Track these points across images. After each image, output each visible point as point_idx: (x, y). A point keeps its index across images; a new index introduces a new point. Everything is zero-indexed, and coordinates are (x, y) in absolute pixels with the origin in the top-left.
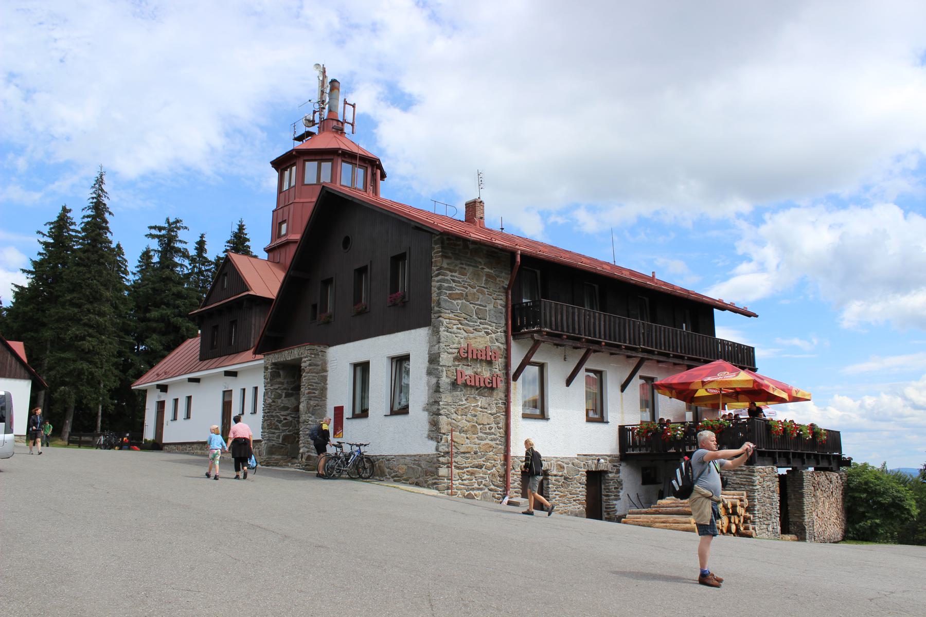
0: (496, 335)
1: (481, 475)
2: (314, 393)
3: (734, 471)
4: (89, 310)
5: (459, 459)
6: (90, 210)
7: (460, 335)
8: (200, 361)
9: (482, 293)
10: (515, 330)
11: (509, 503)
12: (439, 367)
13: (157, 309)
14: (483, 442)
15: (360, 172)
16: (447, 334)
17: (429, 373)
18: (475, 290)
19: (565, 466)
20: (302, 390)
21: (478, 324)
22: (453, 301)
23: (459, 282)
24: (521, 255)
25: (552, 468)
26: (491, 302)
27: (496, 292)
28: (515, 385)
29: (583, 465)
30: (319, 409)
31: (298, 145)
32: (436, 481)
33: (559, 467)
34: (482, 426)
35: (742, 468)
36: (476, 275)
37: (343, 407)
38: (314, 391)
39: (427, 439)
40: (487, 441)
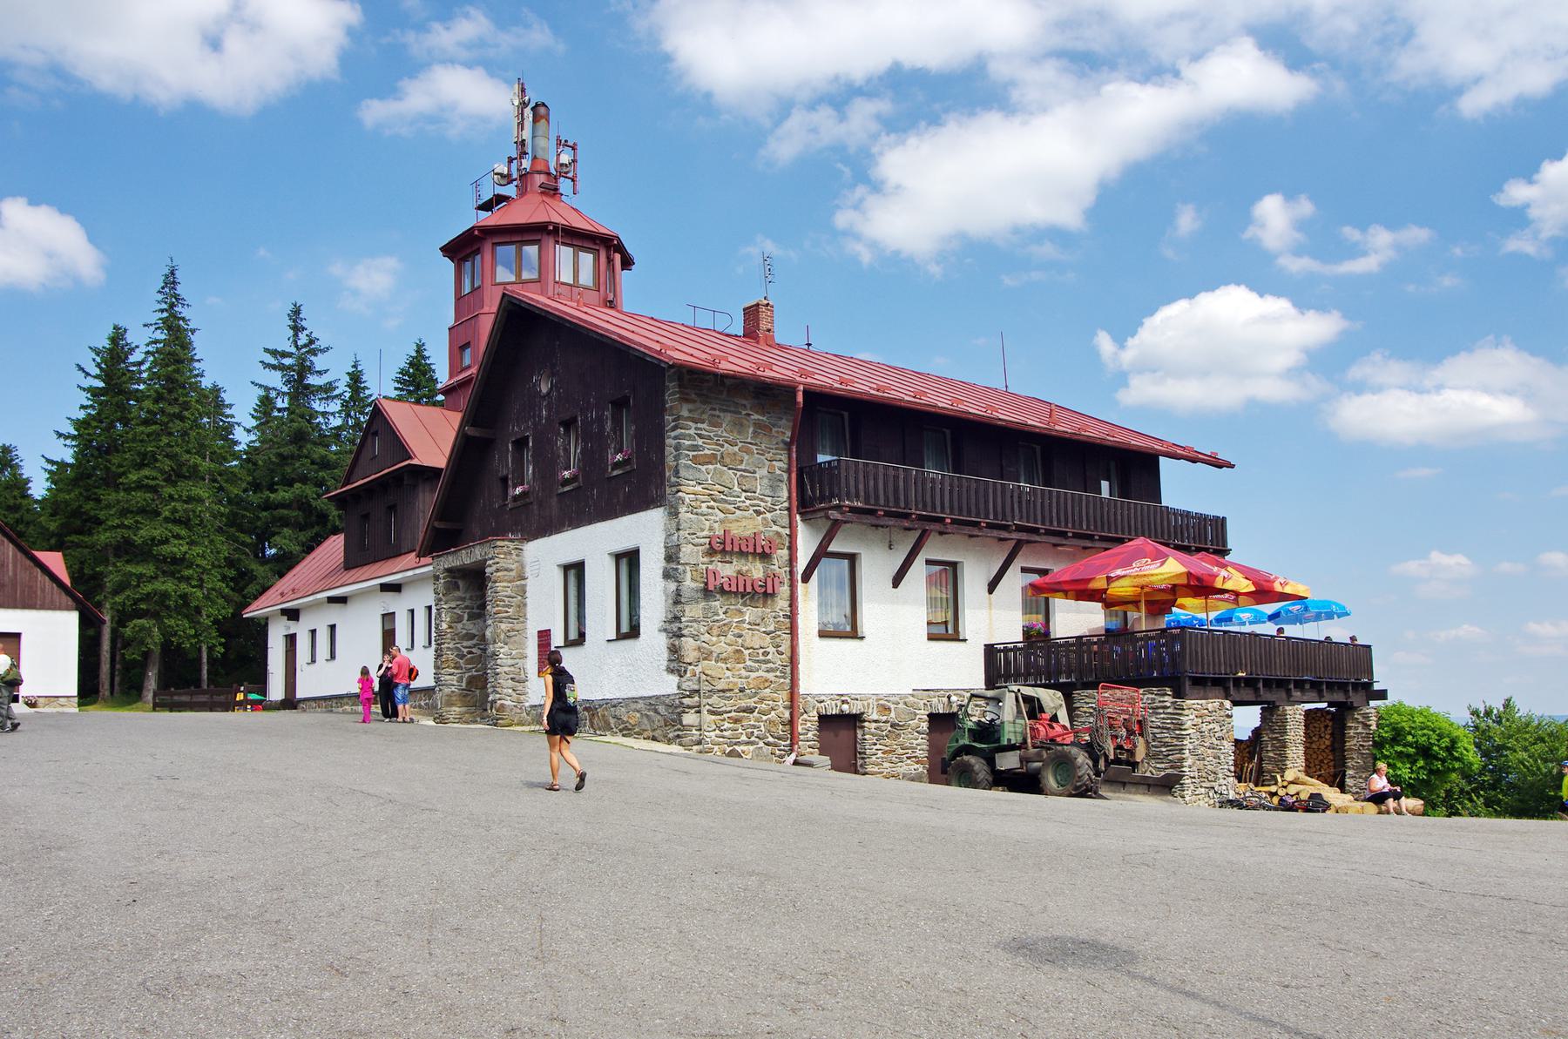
0: (772, 514)
1: (752, 723)
2: (507, 612)
3: (1152, 708)
4: (171, 497)
5: (714, 699)
6: (159, 331)
7: (712, 518)
8: (346, 570)
9: (749, 452)
10: (805, 505)
11: (796, 763)
12: (679, 567)
13: (286, 488)
14: (753, 675)
15: (587, 259)
16: (692, 516)
17: (667, 575)
18: (736, 449)
19: (892, 706)
20: (488, 607)
21: (743, 499)
22: (700, 467)
23: (710, 438)
24: (805, 392)
25: (870, 710)
26: (764, 464)
27: (772, 449)
28: (806, 588)
29: (922, 705)
30: (516, 635)
31: (485, 218)
32: (680, 733)
33: (881, 709)
34: (751, 650)
35: (1166, 704)
36: (739, 426)
37: (550, 630)
38: (507, 609)
39: (666, 673)
40: (761, 673)
